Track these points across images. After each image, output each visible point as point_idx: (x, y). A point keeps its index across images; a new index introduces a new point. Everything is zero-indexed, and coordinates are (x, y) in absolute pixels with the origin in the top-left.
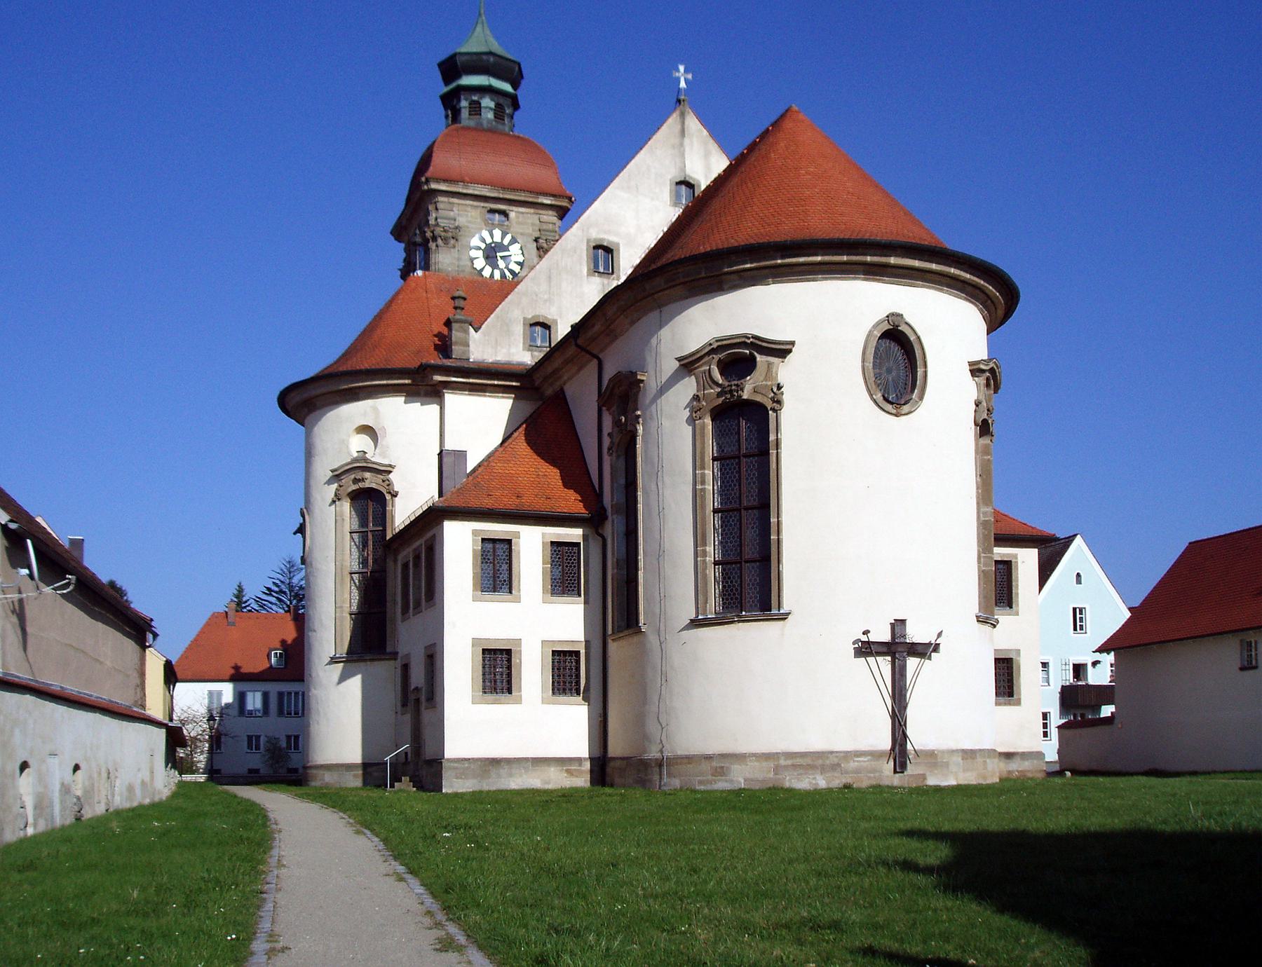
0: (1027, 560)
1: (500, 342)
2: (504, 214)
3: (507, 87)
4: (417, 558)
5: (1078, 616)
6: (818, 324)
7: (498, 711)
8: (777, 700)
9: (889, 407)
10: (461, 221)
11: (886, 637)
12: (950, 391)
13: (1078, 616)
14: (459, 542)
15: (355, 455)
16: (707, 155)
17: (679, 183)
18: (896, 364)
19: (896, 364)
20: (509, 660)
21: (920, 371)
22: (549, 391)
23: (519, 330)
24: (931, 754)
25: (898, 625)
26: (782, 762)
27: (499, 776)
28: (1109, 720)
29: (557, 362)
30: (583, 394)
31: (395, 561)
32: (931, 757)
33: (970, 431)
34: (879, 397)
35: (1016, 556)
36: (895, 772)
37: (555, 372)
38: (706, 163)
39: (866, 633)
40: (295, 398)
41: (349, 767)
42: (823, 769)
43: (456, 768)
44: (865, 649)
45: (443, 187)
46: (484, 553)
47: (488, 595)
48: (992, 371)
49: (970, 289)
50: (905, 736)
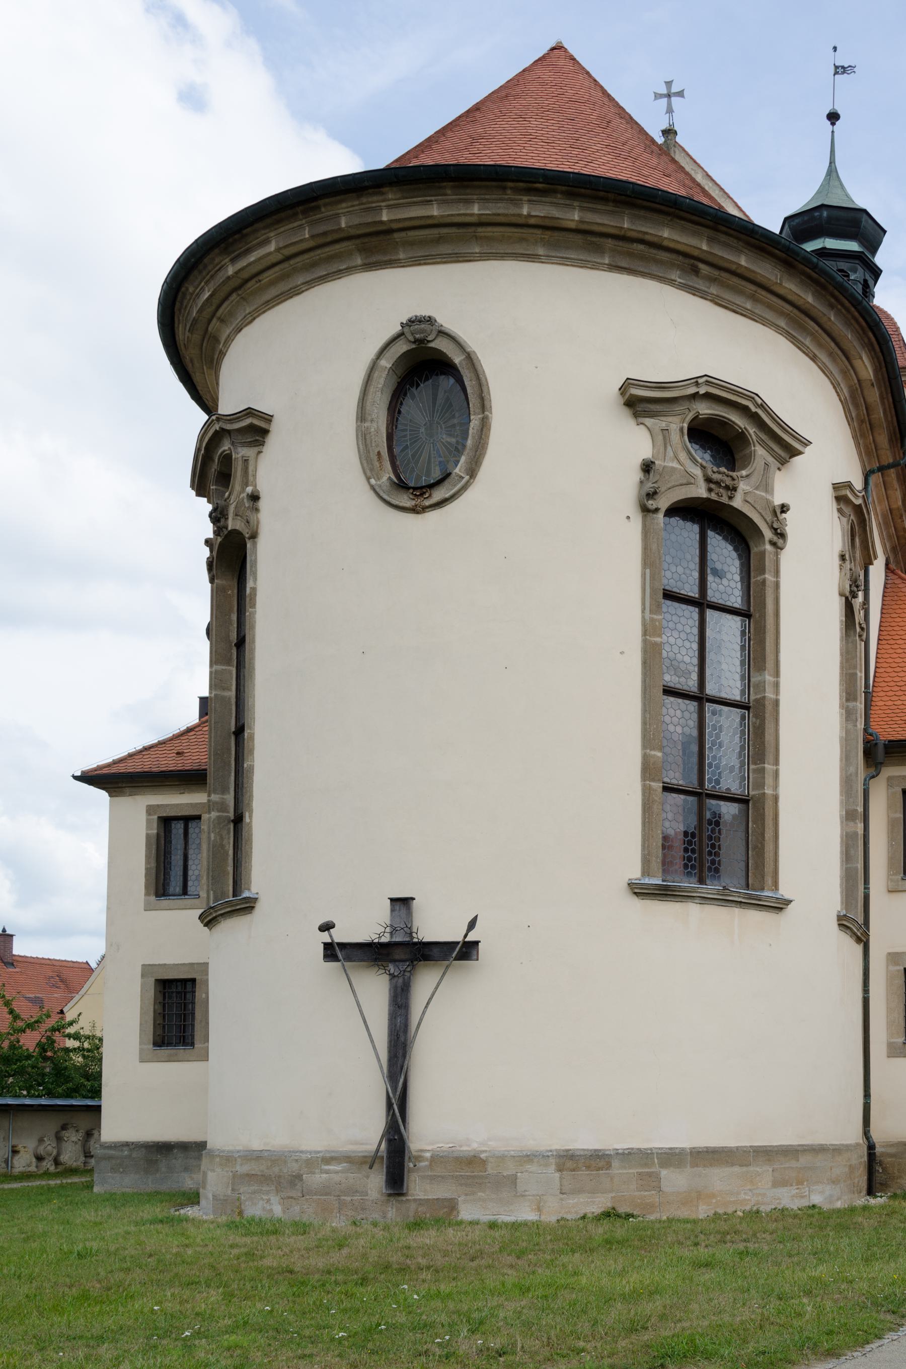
3: (853, 246)
9: (405, 500)
32: (470, 1167)
43: (110, 1158)
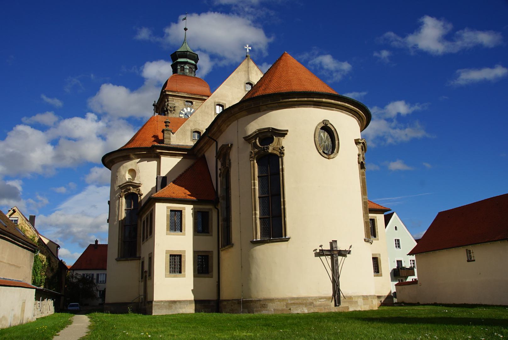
0: (380, 218)
1: (183, 138)
2: (192, 103)
3: (193, 62)
4: (147, 219)
5: (398, 243)
6: (298, 125)
7: (176, 280)
8: (290, 275)
9: (325, 156)
10: (177, 105)
11: (329, 248)
12: (348, 151)
13: (398, 243)
14: (161, 211)
15: (127, 180)
16: (257, 74)
17: (247, 83)
18: (328, 141)
19: (328, 141)
20: (180, 259)
21: (337, 142)
22: (200, 156)
23: (189, 133)
24: (350, 298)
25: (333, 243)
26: (289, 302)
27: (176, 308)
28: (415, 282)
29: (202, 144)
30: (211, 155)
31: (141, 221)
32: (350, 299)
33: (357, 167)
34: (321, 151)
35: (376, 217)
36: (336, 305)
37: (202, 147)
38: (256, 76)
39: (321, 246)
40: (107, 160)
41: (327, 298)
42: (306, 305)
44: (321, 253)
45: (170, 93)
46: (171, 215)
47: (172, 233)
48: (363, 143)
49: (353, 112)
50: (339, 290)
